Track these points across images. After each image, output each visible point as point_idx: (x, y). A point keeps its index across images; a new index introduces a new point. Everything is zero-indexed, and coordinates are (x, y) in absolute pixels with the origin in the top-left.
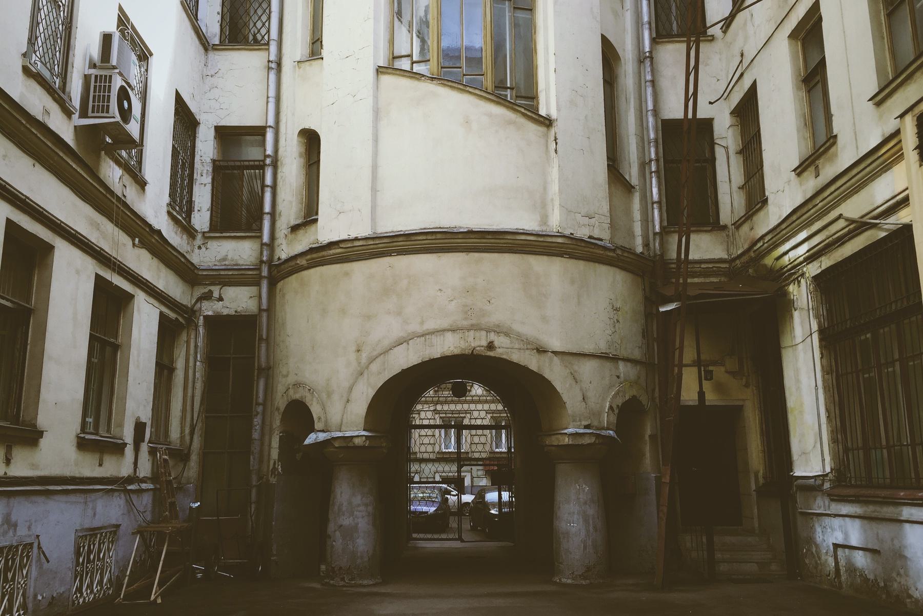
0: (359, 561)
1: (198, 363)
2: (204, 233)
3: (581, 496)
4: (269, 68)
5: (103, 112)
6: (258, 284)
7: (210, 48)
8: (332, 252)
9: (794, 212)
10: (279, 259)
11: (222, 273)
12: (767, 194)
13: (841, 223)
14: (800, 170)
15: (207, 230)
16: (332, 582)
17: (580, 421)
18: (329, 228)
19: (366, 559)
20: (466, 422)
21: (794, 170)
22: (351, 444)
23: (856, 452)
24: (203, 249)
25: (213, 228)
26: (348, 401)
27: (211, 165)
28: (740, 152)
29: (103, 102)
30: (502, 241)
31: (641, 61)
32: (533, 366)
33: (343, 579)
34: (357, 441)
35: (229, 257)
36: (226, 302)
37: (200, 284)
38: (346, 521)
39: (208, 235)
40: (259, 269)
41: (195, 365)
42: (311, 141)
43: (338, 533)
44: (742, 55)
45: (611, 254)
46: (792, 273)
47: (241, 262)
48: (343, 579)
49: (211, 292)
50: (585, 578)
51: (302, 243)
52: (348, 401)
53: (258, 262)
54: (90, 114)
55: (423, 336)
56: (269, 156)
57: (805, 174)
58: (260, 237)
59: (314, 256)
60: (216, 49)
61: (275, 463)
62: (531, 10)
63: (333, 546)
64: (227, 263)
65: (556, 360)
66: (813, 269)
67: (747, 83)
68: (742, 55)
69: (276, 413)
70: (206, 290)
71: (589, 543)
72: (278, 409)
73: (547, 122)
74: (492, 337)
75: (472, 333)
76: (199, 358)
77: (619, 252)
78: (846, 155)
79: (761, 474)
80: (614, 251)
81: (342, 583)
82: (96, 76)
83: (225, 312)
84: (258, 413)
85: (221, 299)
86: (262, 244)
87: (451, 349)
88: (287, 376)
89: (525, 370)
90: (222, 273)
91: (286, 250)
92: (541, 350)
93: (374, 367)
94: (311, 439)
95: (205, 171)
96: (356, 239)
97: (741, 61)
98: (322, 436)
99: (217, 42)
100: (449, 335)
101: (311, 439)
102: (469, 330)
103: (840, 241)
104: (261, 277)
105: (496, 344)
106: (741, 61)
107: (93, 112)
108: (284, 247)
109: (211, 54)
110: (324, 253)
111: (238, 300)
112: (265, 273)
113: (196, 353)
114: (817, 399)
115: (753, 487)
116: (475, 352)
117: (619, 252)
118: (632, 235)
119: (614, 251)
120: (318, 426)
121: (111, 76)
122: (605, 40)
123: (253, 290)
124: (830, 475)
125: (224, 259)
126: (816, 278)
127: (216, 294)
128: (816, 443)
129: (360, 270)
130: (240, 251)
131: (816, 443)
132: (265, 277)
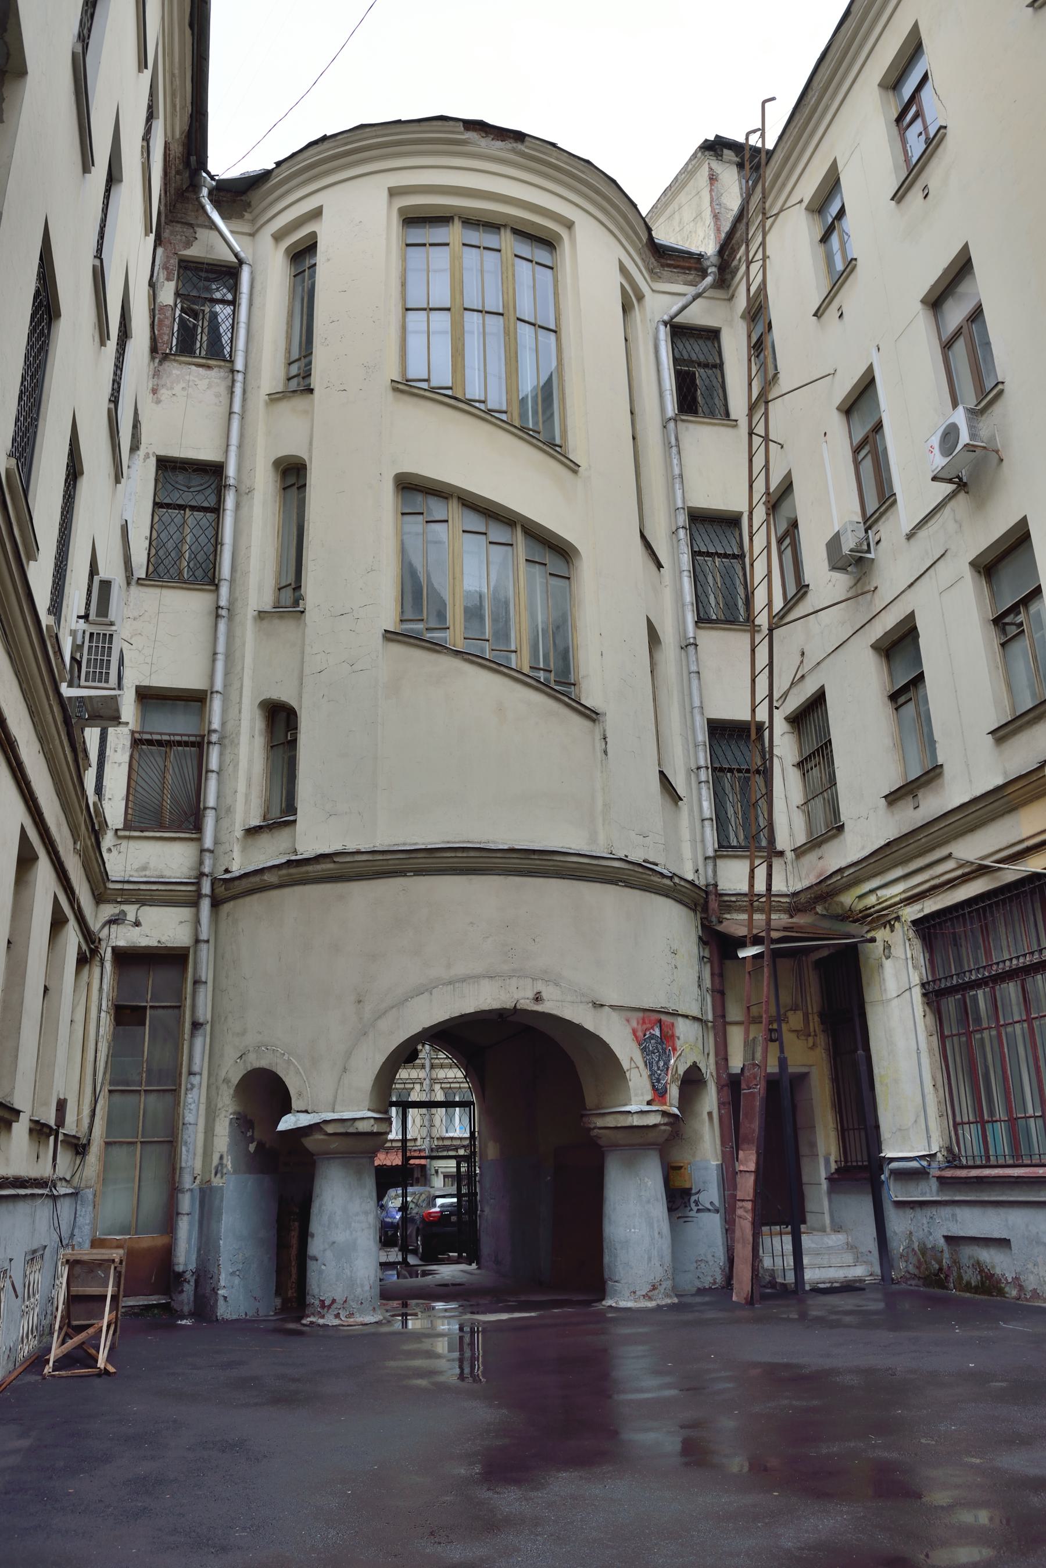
0: (359, 1290)
1: (103, 1014)
2: (117, 830)
3: (643, 1193)
4: (218, 616)
5: (100, 681)
6: (194, 903)
7: (134, 582)
8: (319, 867)
9: (888, 844)
10: (227, 871)
11: (143, 887)
12: (842, 819)
13: (950, 865)
14: (893, 798)
15: (121, 826)
16: (321, 1321)
17: (642, 1095)
18: (313, 836)
19: (367, 1288)
20: (414, 1097)
21: (885, 797)
22: (351, 1130)
23: (966, 1127)
24: (115, 852)
25: (127, 826)
26: (345, 1070)
27: (129, 737)
28: (800, 765)
29: (101, 667)
30: (551, 863)
31: (684, 648)
32: (589, 1026)
33: (337, 1316)
34: (363, 1127)
35: (152, 865)
36: (144, 928)
37: (108, 902)
38: (341, 1236)
39: (120, 833)
40: (198, 884)
41: (99, 1018)
42: (281, 720)
43: (329, 1254)
44: (803, 654)
45: (667, 882)
46: (882, 917)
47: (167, 873)
48: (337, 1316)
49: (123, 913)
50: (650, 1299)
51: (269, 852)
52: (345, 1070)
53: (194, 873)
54: (83, 683)
55: (450, 983)
56: (215, 731)
57: (901, 804)
58: (199, 840)
59: (293, 871)
60: (142, 585)
61: (221, 1158)
62: (569, 578)
63: (321, 1272)
64: (147, 873)
65: (615, 1016)
66: (912, 913)
67: (808, 689)
68: (803, 654)
69: (224, 1087)
70: (117, 911)
71: (655, 1253)
72: (226, 1081)
73: (592, 715)
74: (540, 986)
75: (514, 981)
76: (104, 1007)
77: (676, 880)
78: (955, 791)
79: (832, 1159)
80: (671, 878)
81: (336, 1322)
82: (92, 634)
83: (144, 942)
84: (193, 1086)
85: (137, 924)
86: (202, 851)
87: (489, 1001)
88: (244, 1033)
89: (579, 1029)
90: (143, 887)
91: (239, 861)
92: (598, 1006)
93: (383, 1025)
94: (287, 1123)
95: (120, 746)
96: (359, 852)
97: (802, 662)
98: (304, 1120)
99: (144, 576)
100: (485, 984)
101: (287, 1123)
102: (510, 977)
103: (952, 884)
104: (199, 896)
105: (544, 995)
106: (802, 662)
107: (86, 680)
108: (236, 854)
109: (134, 589)
110: (310, 868)
111: (162, 927)
112: (206, 888)
113: (100, 1000)
114: (919, 1064)
115: (823, 1174)
116: (518, 1007)
117: (676, 880)
118: (680, 859)
119: (671, 878)
120: (295, 1104)
121: (111, 635)
122: (649, 621)
123: (185, 913)
124: (939, 1154)
125: (144, 868)
126: (914, 923)
127: (131, 917)
128: (918, 1116)
129: (362, 895)
130: (167, 859)
131: (918, 1116)
132: (206, 896)
